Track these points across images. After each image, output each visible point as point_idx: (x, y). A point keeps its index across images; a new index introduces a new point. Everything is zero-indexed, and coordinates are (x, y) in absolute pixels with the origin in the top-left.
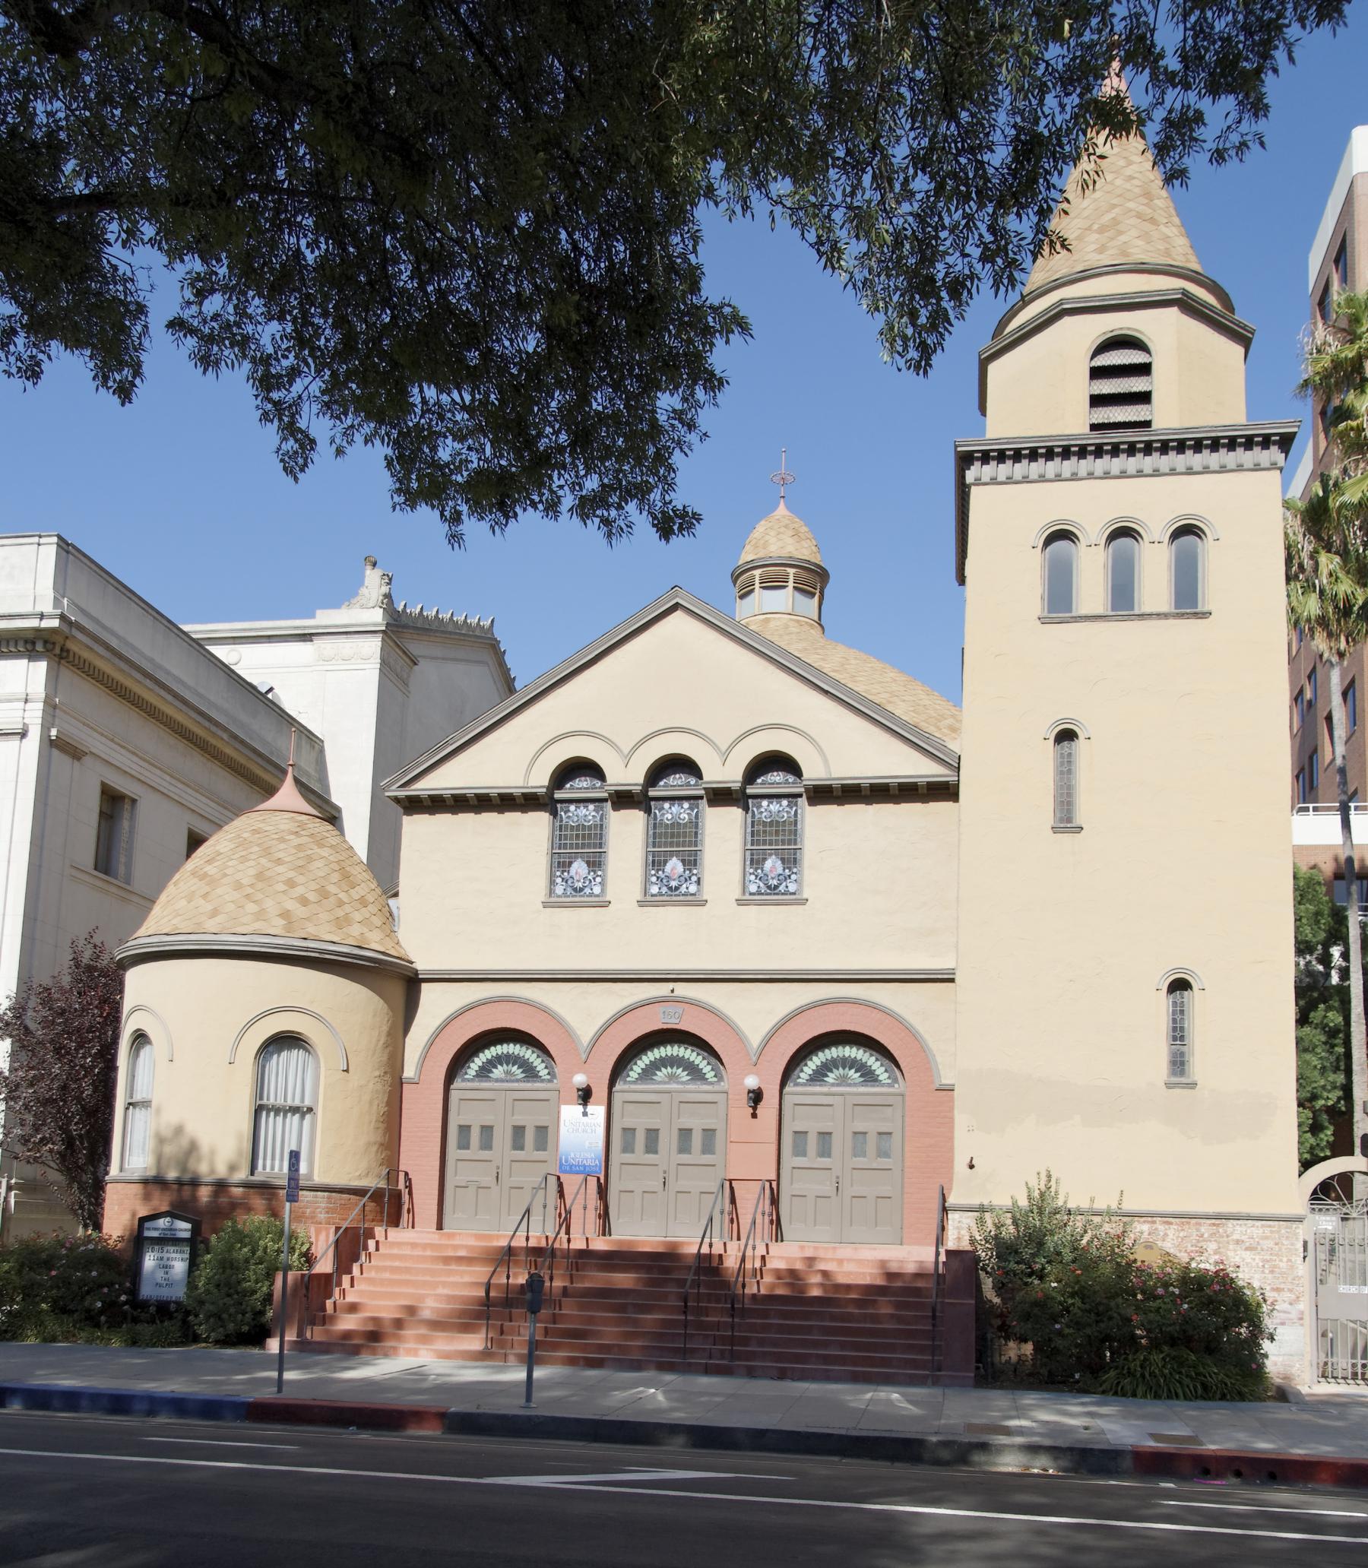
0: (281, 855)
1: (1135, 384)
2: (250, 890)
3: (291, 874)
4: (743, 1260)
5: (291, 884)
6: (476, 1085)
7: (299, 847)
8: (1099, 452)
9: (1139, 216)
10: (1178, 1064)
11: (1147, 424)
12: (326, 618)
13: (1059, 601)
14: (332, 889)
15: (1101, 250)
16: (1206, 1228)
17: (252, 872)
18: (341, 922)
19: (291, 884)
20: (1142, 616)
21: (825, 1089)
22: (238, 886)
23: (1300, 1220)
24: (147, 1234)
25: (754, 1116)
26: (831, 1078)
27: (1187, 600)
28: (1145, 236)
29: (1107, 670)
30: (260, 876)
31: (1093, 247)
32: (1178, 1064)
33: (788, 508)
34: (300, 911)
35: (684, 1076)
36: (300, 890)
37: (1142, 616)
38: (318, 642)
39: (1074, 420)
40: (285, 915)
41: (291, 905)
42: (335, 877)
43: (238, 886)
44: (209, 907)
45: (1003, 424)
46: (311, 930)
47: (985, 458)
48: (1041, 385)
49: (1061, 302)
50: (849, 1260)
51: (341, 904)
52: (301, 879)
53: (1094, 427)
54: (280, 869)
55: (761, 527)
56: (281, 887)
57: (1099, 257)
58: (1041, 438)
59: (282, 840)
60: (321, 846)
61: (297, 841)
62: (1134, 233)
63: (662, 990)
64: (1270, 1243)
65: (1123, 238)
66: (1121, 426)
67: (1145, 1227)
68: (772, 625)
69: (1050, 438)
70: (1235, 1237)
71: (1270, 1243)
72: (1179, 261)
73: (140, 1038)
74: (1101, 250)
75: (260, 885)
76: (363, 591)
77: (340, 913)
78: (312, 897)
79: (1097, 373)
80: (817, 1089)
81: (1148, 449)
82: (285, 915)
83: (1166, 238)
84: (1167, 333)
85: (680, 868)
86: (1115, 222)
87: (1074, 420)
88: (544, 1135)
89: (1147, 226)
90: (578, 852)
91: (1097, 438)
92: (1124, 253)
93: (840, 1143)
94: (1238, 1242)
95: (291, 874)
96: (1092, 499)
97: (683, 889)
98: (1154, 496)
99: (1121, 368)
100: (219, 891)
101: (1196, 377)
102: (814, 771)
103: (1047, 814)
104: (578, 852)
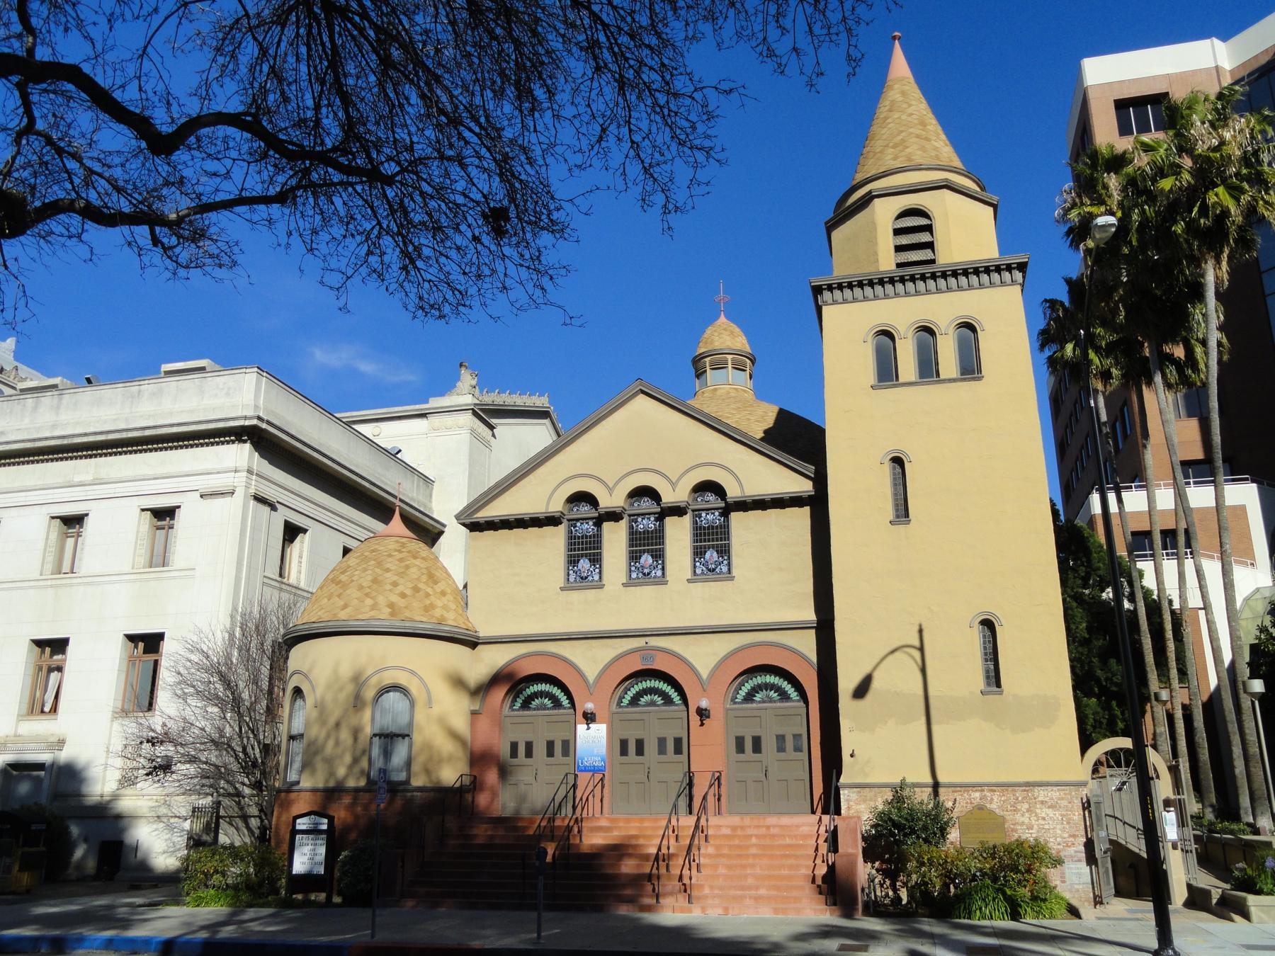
0: (388, 566)
1: (905, 240)
2: (368, 590)
3: (395, 578)
4: (659, 849)
5: (395, 584)
6: (521, 713)
7: (401, 560)
8: (902, 280)
9: (918, 136)
10: (994, 678)
11: (933, 261)
12: (435, 403)
13: (887, 372)
14: (421, 586)
15: (895, 158)
16: (1019, 794)
17: (370, 578)
18: (427, 609)
19: (395, 584)
20: (944, 381)
21: (754, 705)
22: (361, 588)
23: (1084, 784)
24: (298, 827)
25: (702, 725)
26: (758, 697)
27: (971, 368)
28: (923, 149)
29: (918, 417)
30: (375, 581)
31: (890, 157)
32: (994, 678)
33: (727, 317)
34: (401, 603)
35: (659, 700)
36: (400, 588)
37: (944, 381)
38: (432, 418)
39: (887, 261)
40: (391, 605)
41: (394, 598)
42: (424, 578)
43: (361, 588)
44: (342, 603)
45: (842, 268)
46: (407, 614)
47: (830, 288)
48: (873, 239)
49: (946, 180)
50: (774, 826)
51: (428, 595)
52: (401, 581)
53: (899, 265)
54: (388, 575)
55: (709, 331)
56: (388, 587)
57: (892, 162)
58: (854, 276)
59: (390, 556)
60: (415, 558)
61: (399, 556)
62: (915, 147)
63: (639, 643)
64: (1064, 803)
65: (908, 150)
66: (919, 265)
67: (977, 795)
68: (719, 393)
69: (870, 274)
70: (1040, 799)
71: (1064, 803)
72: (944, 162)
73: (298, 692)
74: (895, 158)
75: (375, 586)
76: (459, 384)
77: (428, 602)
78: (408, 592)
79: (897, 232)
80: (749, 706)
81: (934, 276)
82: (391, 605)
83: (936, 149)
84: (943, 206)
85: (650, 560)
86: (903, 141)
87: (887, 261)
88: (568, 747)
89: (924, 142)
90: (584, 551)
91: (902, 272)
92: (910, 160)
93: (769, 744)
94: (1042, 802)
95: (395, 578)
96: (903, 311)
97: (653, 574)
98: (943, 308)
99: (916, 228)
100: (348, 592)
101: (966, 230)
102: (733, 492)
103: (890, 513)
104: (584, 551)
